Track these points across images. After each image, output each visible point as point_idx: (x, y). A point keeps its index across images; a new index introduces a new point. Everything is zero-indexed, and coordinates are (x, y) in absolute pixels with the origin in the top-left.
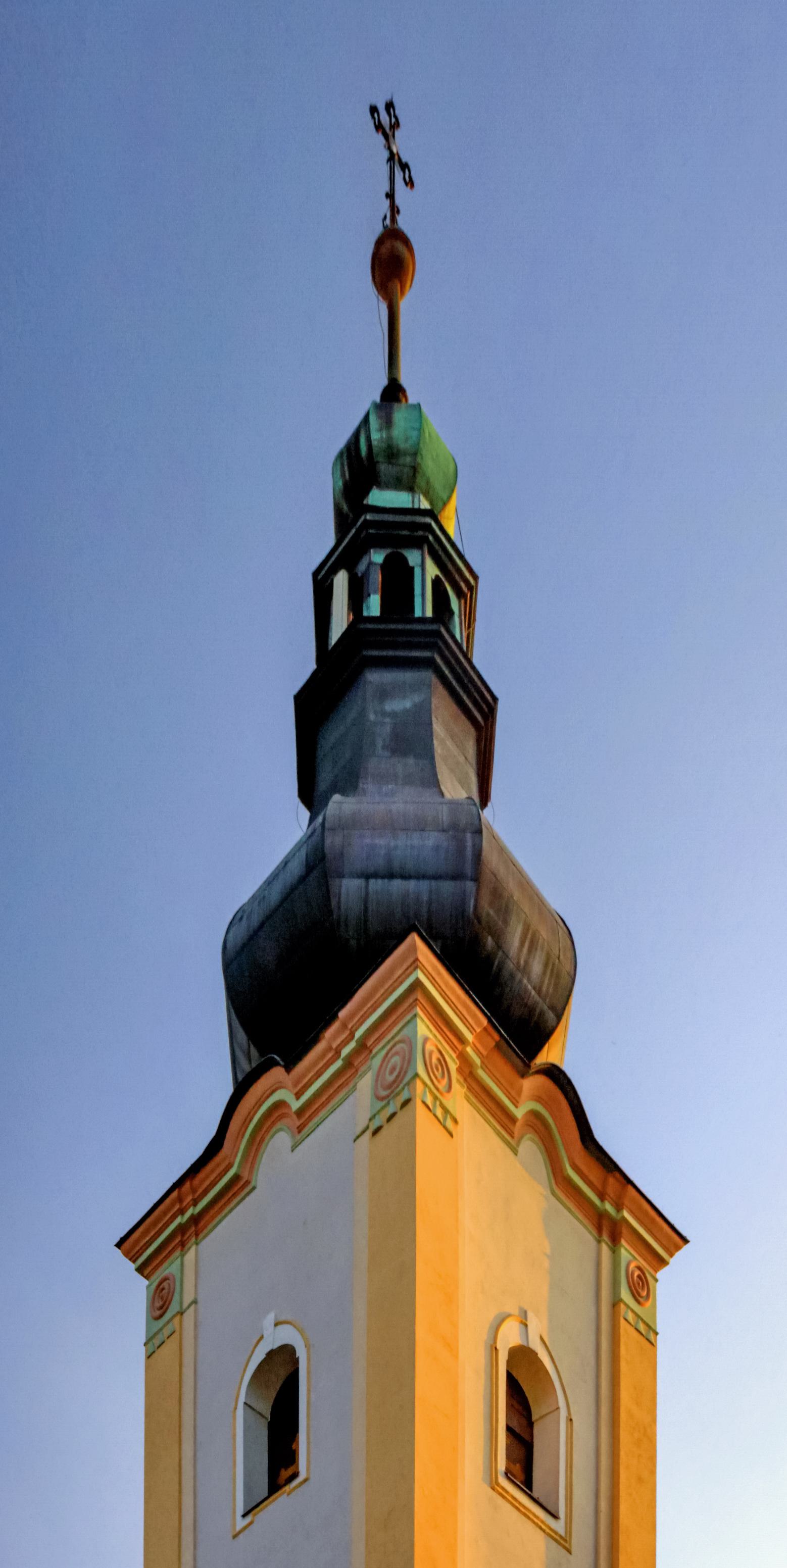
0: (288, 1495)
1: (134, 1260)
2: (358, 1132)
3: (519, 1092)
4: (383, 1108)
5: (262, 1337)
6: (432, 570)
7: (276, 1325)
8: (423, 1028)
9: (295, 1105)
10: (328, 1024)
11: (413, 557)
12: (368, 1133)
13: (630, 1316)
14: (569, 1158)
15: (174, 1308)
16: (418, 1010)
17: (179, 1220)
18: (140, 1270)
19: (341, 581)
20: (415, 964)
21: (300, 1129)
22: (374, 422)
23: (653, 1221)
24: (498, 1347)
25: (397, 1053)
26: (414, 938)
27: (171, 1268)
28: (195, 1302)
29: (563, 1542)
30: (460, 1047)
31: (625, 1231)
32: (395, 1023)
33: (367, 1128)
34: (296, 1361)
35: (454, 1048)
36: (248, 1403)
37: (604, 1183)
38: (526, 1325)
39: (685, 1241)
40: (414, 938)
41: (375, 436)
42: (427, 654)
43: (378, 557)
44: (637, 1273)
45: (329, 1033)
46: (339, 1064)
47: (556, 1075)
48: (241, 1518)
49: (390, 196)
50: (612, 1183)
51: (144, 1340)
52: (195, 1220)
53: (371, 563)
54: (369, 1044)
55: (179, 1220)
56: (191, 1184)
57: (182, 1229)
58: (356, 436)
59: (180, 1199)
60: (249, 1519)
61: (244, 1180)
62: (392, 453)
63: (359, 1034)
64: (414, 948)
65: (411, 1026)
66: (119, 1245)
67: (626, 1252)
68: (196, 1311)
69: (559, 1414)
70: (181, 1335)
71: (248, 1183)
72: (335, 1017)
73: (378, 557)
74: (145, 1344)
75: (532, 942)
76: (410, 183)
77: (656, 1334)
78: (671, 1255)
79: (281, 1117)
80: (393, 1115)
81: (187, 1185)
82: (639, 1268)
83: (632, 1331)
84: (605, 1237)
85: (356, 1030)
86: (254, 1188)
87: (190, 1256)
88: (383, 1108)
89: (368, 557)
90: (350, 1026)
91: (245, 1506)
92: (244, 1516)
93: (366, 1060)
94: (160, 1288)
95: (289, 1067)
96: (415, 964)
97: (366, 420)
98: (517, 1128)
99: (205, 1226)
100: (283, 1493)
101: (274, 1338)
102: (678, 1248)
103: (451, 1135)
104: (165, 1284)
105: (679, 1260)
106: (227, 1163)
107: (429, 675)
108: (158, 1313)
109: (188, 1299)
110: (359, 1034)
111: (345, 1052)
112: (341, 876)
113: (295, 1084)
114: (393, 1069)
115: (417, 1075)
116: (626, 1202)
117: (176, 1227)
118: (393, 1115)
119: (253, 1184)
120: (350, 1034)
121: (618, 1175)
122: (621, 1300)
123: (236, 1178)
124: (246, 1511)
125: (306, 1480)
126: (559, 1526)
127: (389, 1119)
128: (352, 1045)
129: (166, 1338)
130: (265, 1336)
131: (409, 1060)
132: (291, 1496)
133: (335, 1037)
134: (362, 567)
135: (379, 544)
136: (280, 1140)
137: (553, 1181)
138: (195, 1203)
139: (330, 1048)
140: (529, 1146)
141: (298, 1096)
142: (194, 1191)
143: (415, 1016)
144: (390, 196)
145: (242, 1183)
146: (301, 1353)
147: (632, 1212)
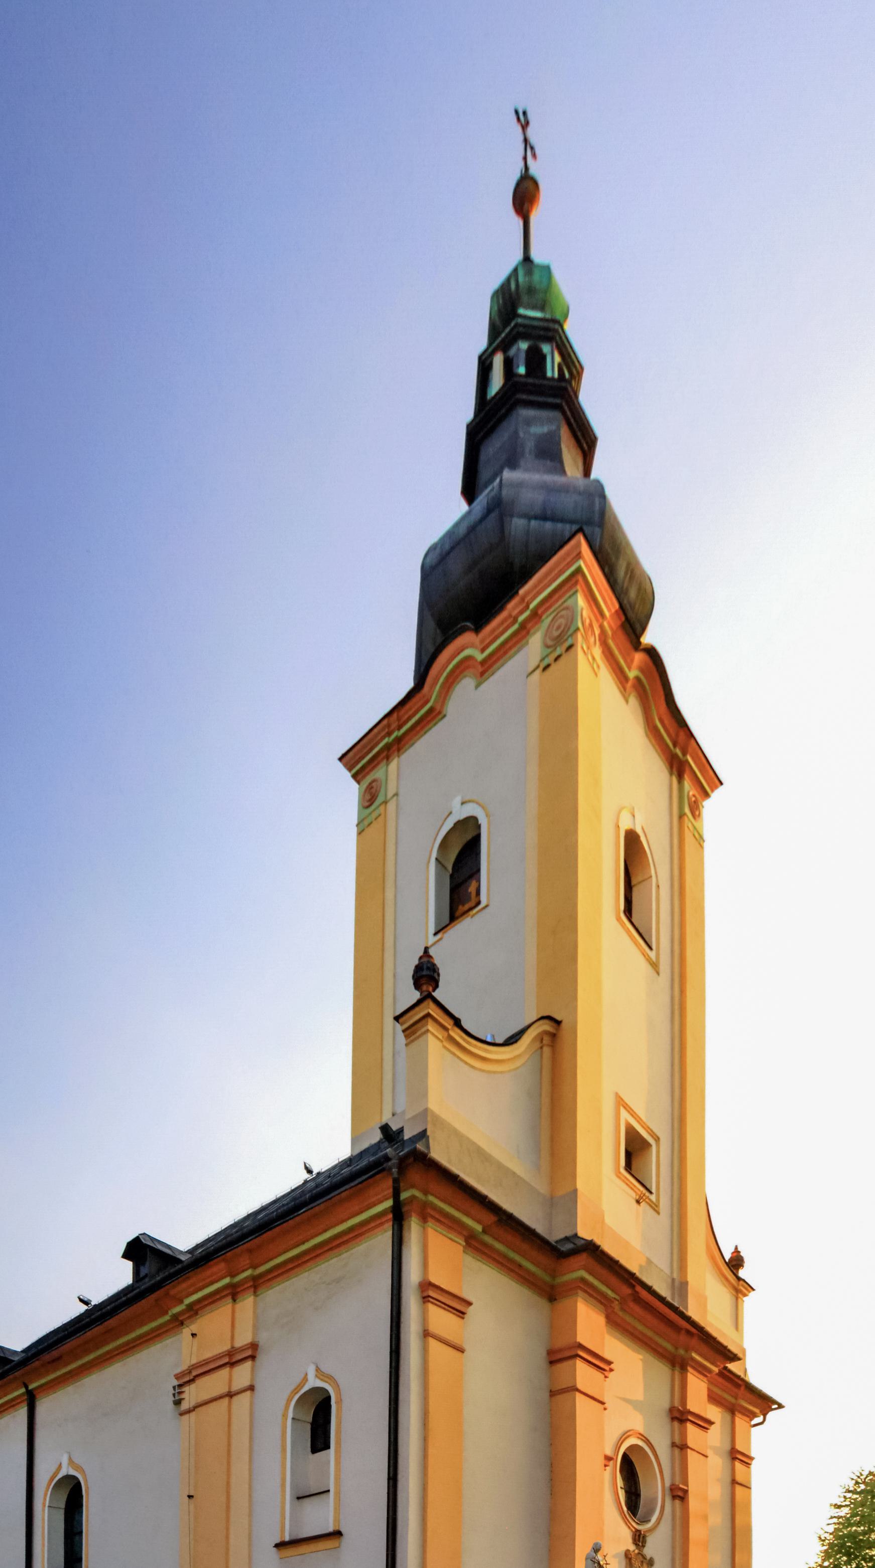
0: (472, 917)
1: (350, 770)
2: (531, 669)
3: (632, 661)
4: (551, 652)
5: (451, 813)
6: (558, 359)
7: (463, 803)
8: (581, 601)
9: (480, 657)
10: (512, 597)
11: (546, 348)
12: (538, 672)
13: (690, 825)
14: (658, 714)
15: (380, 799)
16: (578, 587)
17: (386, 740)
18: (355, 777)
19: (498, 360)
20: (579, 556)
21: (482, 674)
22: (521, 273)
23: (704, 766)
24: (620, 826)
25: (562, 617)
26: (580, 538)
27: (378, 773)
28: (396, 794)
29: (655, 966)
30: (601, 620)
31: (687, 769)
32: (560, 598)
33: (538, 667)
34: (479, 827)
35: (597, 620)
36: (439, 858)
37: (677, 735)
38: (634, 816)
39: (721, 783)
40: (580, 538)
41: (521, 279)
42: (558, 401)
43: (524, 345)
44: (693, 799)
45: (510, 606)
46: (516, 626)
47: (652, 653)
48: (433, 936)
49: (525, 158)
50: (682, 736)
51: (356, 822)
52: (399, 740)
53: (519, 349)
54: (540, 612)
55: (386, 740)
56: (398, 715)
57: (388, 747)
58: (508, 280)
59: (389, 725)
60: (439, 936)
61: (438, 711)
62: (531, 290)
63: (532, 606)
64: (579, 544)
65: (574, 596)
66: (340, 759)
67: (687, 784)
68: (397, 800)
69: (652, 880)
70: (385, 817)
71: (440, 713)
72: (517, 593)
73: (524, 345)
74: (357, 825)
75: (630, 577)
76: (534, 156)
77: (704, 841)
78: (712, 791)
79: (468, 667)
80: (548, 666)
81: (395, 715)
82: (694, 796)
83: (691, 835)
84: (675, 772)
85: (531, 602)
86: (445, 716)
87: (393, 765)
88: (551, 652)
89: (517, 345)
90: (526, 601)
91: (436, 927)
92: (435, 934)
93: (536, 623)
94: (370, 787)
95: (477, 629)
96: (579, 556)
97: (515, 270)
98: (629, 685)
99: (404, 745)
100: (468, 916)
101: (461, 813)
102: (716, 787)
103: (596, 674)
104: (374, 784)
105: (717, 795)
106: (425, 699)
107: (557, 414)
108: (367, 804)
109: (390, 794)
110: (532, 606)
111: (521, 618)
112: (512, 516)
113: (482, 641)
114: (558, 628)
115: (578, 629)
116: (690, 750)
117: (384, 746)
118: (548, 666)
119: (444, 713)
120: (526, 606)
121: (686, 728)
122: (685, 814)
123: (431, 710)
124: (437, 931)
125: (487, 906)
126: (652, 955)
127: (556, 659)
128: (527, 614)
129: (373, 819)
130: (454, 812)
131: (572, 619)
132: (474, 918)
133: (514, 608)
134: (512, 352)
135: (525, 336)
136: (467, 684)
137: (647, 727)
138: (399, 728)
139: (510, 616)
140: (633, 701)
141: (483, 651)
142: (399, 719)
143: (576, 592)
144: (525, 158)
145: (434, 714)
146: (483, 821)
147: (693, 758)
